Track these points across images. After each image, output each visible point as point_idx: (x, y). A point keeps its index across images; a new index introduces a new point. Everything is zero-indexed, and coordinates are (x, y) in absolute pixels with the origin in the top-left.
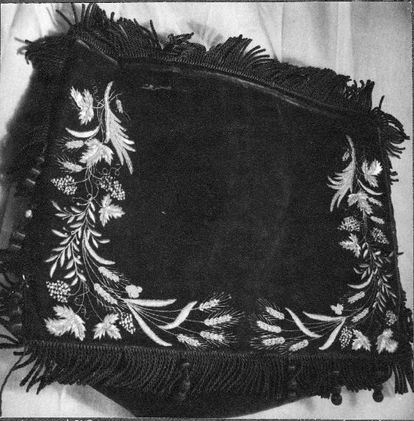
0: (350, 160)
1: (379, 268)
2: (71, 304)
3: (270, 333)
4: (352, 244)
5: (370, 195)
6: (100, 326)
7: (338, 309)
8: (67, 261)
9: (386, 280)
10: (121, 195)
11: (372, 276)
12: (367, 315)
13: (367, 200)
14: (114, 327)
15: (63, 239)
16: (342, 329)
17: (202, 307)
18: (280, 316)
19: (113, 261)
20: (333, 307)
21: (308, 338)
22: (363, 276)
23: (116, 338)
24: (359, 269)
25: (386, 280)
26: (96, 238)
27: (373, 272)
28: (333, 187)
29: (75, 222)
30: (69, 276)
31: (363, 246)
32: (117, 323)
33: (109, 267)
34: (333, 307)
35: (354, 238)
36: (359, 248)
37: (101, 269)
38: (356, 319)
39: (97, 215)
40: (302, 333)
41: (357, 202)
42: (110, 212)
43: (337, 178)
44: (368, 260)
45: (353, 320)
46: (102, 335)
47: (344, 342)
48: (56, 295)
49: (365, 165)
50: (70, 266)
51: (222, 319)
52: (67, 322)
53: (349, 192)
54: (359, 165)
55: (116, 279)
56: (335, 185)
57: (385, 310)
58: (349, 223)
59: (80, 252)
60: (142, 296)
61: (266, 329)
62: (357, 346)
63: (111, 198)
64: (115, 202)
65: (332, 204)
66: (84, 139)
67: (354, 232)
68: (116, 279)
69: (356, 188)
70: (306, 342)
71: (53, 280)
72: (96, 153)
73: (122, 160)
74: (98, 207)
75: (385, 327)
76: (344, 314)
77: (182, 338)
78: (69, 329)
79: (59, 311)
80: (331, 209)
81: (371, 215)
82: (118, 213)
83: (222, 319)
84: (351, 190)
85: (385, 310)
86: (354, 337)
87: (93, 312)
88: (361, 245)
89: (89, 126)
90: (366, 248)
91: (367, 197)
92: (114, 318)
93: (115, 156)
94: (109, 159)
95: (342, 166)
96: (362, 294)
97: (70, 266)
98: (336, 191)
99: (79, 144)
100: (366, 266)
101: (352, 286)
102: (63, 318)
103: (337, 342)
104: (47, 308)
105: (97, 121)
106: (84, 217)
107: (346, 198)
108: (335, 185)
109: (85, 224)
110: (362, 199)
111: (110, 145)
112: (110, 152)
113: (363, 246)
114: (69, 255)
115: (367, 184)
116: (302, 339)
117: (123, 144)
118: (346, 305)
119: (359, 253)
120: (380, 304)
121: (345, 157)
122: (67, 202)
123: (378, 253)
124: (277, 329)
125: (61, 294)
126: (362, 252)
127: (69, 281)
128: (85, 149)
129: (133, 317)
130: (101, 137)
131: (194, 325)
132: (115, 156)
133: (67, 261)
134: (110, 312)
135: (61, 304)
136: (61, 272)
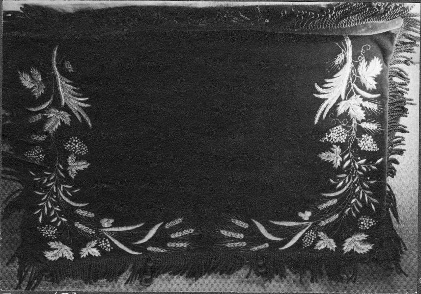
0: (345, 61)
1: (360, 175)
2: (58, 239)
3: (235, 238)
4: (334, 157)
5: (365, 99)
6: (84, 250)
7: (307, 215)
8: (49, 210)
9: (367, 186)
10: (85, 150)
11: (348, 185)
12: (336, 219)
13: (361, 105)
14: (95, 250)
15: (43, 196)
16: (307, 231)
17: (167, 226)
18: (246, 226)
19: (87, 203)
20: (300, 214)
21: (269, 241)
22: (338, 186)
23: (97, 255)
24: (335, 179)
25: (367, 186)
26: (69, 190)
27: (351, 180)
28: (321, 96)
29: (48, 182)
30: (54, 220)
31: (346, 156)
32: (97, 247)
33: (82, 209)
34: (300, 214)
35: (337, 149)
36: (340, 159)
37: (79, 212)
38: (323, 223)
39: (65, 172)
40: (264, 238)
41: (348, 110)
42: (76, 167)
43: (325, 86)
44: (349, 171)
45: (320, 224)
46: (86, 255)
47: (307, 243)
48: (47, 235)
49: (363, 64)
50: (53, 213)
51: (186, 232)
52: (60, 251)
53: (340, 100)
54: (356, 65)
55: (91, 215)
56: (323, 94)
57: (358, 216)
58: (337, 134)
59: (59, 202)
60: (114, 225)
61: (230, 236)
62: (321, 246)
63: (75, 155)
64: (79, 158)
65: (318, 115)
66: (42, 111)
67: (338, 144)
68: (91, 215)
69: (349, 93)
70: (267, 245)
71: (43, 225)
72: (55, 120)
73: (79, 119)
74: (66, 165)
75: (357, 231)
76: (311, 219)
77: (150, 249)
78: (61, 255)
79: (53, 245)
80: (316, 122)
81: (363, 121)
82: (83, 165)
83: (186, 232)
84: (343, 98)
85: (358, 216)
86: (319, 239)
87: (77, 242)
88: (342, 156)
89: (43, 99)
90: (348, 159)
91: (361, 102)
92: (94, 243)
93: (72, 116)
94: (67, 120)
95: (334, 71)
96: (335, 201)
97: (53, 213)
98: (325, 99)
99: (38, 117)
100: (344, 175)
101: (325, 195)
102: (55, 249)
103: (300, 243)
104: (43, 244)
105: (51, 92)
106: (55, 176)
107: (335, 106)
108: (323, 94)
109: (56, 182)
110: (355, 108)
111: (66, 109)
112: (67, 115)
113: (346, 156)
114: (50, 206)
115: (363, 87)
116: (265, 242)
117: (76, 103)
118: (315, 211)
119: (339, 164)
120: (354, 210)
121: (339, 60)
122: (39, 169)
123: (363, 161)
124: (242, 236)
125: (51, 233)
126: (343, 163)
127: (55, 223)
128: (46, 119)
129: (110, 240)
130: (57, 104)
131: (161, 239)
132: (72, 116)
133: (49, 210)
134: (90, 240)
135: (53, 241)
136: (47, 220)
